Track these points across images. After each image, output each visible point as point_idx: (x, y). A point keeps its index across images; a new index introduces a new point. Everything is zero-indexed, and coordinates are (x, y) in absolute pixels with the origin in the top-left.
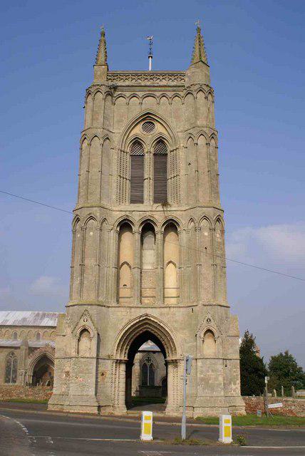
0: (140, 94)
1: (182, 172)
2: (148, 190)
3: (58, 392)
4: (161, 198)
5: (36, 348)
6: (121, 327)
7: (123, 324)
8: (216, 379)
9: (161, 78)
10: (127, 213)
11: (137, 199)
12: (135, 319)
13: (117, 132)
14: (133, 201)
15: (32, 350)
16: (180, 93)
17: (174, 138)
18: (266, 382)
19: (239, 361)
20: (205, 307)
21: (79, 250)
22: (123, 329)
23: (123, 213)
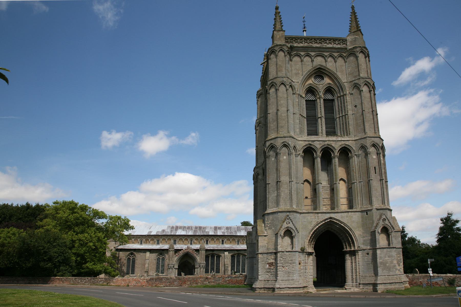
0: (313, 54)
1: (350, 112)
2: (322, 126)
3: (263, 279)
4: (331, 132)
5: (180, 250)
6: (311, 228)
7: (313, 225)
8: (392, 262)
9: (328, 42)
10: (310, 143)
11: (315, 133)
12: (321, 222)
13: (297, 80)
14: (328, 134)
15: (177, 251)
16: (334, 54)
17: (341, 88)
18: (429, 263)
19: (401, 249)
20: (378, 211)
21: (290, 173)
22: (313, 229)
23: (307, 143)
